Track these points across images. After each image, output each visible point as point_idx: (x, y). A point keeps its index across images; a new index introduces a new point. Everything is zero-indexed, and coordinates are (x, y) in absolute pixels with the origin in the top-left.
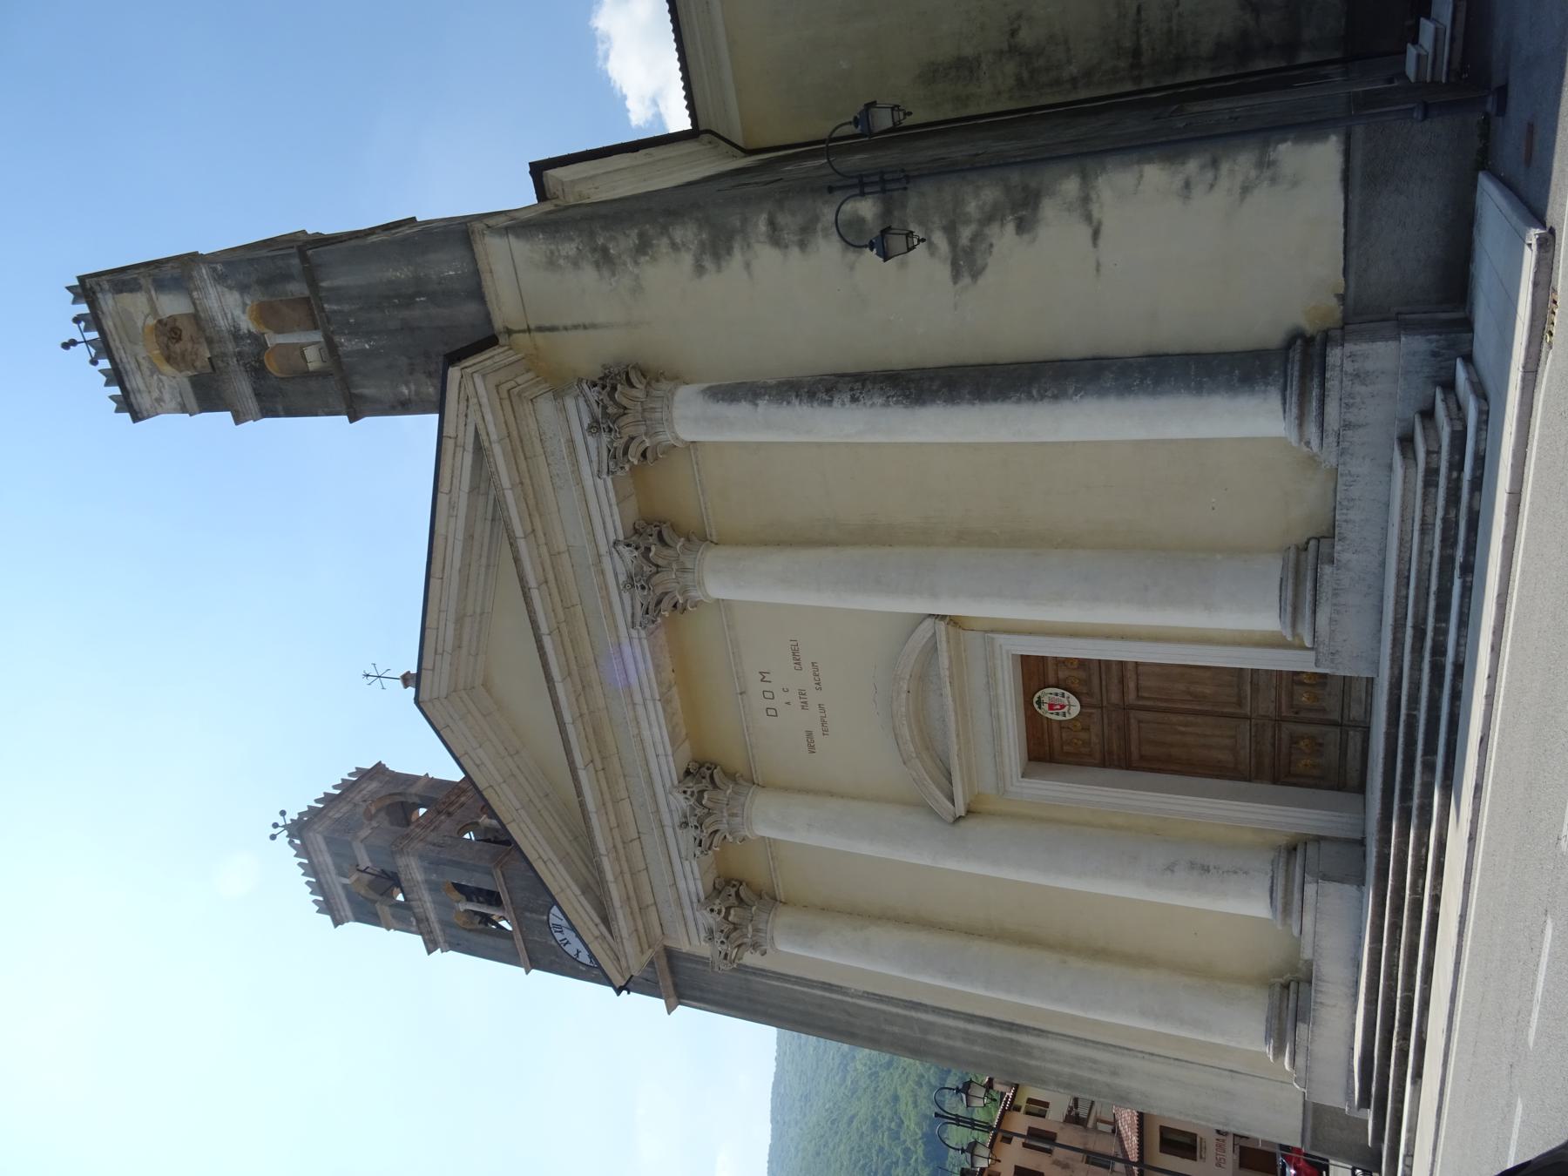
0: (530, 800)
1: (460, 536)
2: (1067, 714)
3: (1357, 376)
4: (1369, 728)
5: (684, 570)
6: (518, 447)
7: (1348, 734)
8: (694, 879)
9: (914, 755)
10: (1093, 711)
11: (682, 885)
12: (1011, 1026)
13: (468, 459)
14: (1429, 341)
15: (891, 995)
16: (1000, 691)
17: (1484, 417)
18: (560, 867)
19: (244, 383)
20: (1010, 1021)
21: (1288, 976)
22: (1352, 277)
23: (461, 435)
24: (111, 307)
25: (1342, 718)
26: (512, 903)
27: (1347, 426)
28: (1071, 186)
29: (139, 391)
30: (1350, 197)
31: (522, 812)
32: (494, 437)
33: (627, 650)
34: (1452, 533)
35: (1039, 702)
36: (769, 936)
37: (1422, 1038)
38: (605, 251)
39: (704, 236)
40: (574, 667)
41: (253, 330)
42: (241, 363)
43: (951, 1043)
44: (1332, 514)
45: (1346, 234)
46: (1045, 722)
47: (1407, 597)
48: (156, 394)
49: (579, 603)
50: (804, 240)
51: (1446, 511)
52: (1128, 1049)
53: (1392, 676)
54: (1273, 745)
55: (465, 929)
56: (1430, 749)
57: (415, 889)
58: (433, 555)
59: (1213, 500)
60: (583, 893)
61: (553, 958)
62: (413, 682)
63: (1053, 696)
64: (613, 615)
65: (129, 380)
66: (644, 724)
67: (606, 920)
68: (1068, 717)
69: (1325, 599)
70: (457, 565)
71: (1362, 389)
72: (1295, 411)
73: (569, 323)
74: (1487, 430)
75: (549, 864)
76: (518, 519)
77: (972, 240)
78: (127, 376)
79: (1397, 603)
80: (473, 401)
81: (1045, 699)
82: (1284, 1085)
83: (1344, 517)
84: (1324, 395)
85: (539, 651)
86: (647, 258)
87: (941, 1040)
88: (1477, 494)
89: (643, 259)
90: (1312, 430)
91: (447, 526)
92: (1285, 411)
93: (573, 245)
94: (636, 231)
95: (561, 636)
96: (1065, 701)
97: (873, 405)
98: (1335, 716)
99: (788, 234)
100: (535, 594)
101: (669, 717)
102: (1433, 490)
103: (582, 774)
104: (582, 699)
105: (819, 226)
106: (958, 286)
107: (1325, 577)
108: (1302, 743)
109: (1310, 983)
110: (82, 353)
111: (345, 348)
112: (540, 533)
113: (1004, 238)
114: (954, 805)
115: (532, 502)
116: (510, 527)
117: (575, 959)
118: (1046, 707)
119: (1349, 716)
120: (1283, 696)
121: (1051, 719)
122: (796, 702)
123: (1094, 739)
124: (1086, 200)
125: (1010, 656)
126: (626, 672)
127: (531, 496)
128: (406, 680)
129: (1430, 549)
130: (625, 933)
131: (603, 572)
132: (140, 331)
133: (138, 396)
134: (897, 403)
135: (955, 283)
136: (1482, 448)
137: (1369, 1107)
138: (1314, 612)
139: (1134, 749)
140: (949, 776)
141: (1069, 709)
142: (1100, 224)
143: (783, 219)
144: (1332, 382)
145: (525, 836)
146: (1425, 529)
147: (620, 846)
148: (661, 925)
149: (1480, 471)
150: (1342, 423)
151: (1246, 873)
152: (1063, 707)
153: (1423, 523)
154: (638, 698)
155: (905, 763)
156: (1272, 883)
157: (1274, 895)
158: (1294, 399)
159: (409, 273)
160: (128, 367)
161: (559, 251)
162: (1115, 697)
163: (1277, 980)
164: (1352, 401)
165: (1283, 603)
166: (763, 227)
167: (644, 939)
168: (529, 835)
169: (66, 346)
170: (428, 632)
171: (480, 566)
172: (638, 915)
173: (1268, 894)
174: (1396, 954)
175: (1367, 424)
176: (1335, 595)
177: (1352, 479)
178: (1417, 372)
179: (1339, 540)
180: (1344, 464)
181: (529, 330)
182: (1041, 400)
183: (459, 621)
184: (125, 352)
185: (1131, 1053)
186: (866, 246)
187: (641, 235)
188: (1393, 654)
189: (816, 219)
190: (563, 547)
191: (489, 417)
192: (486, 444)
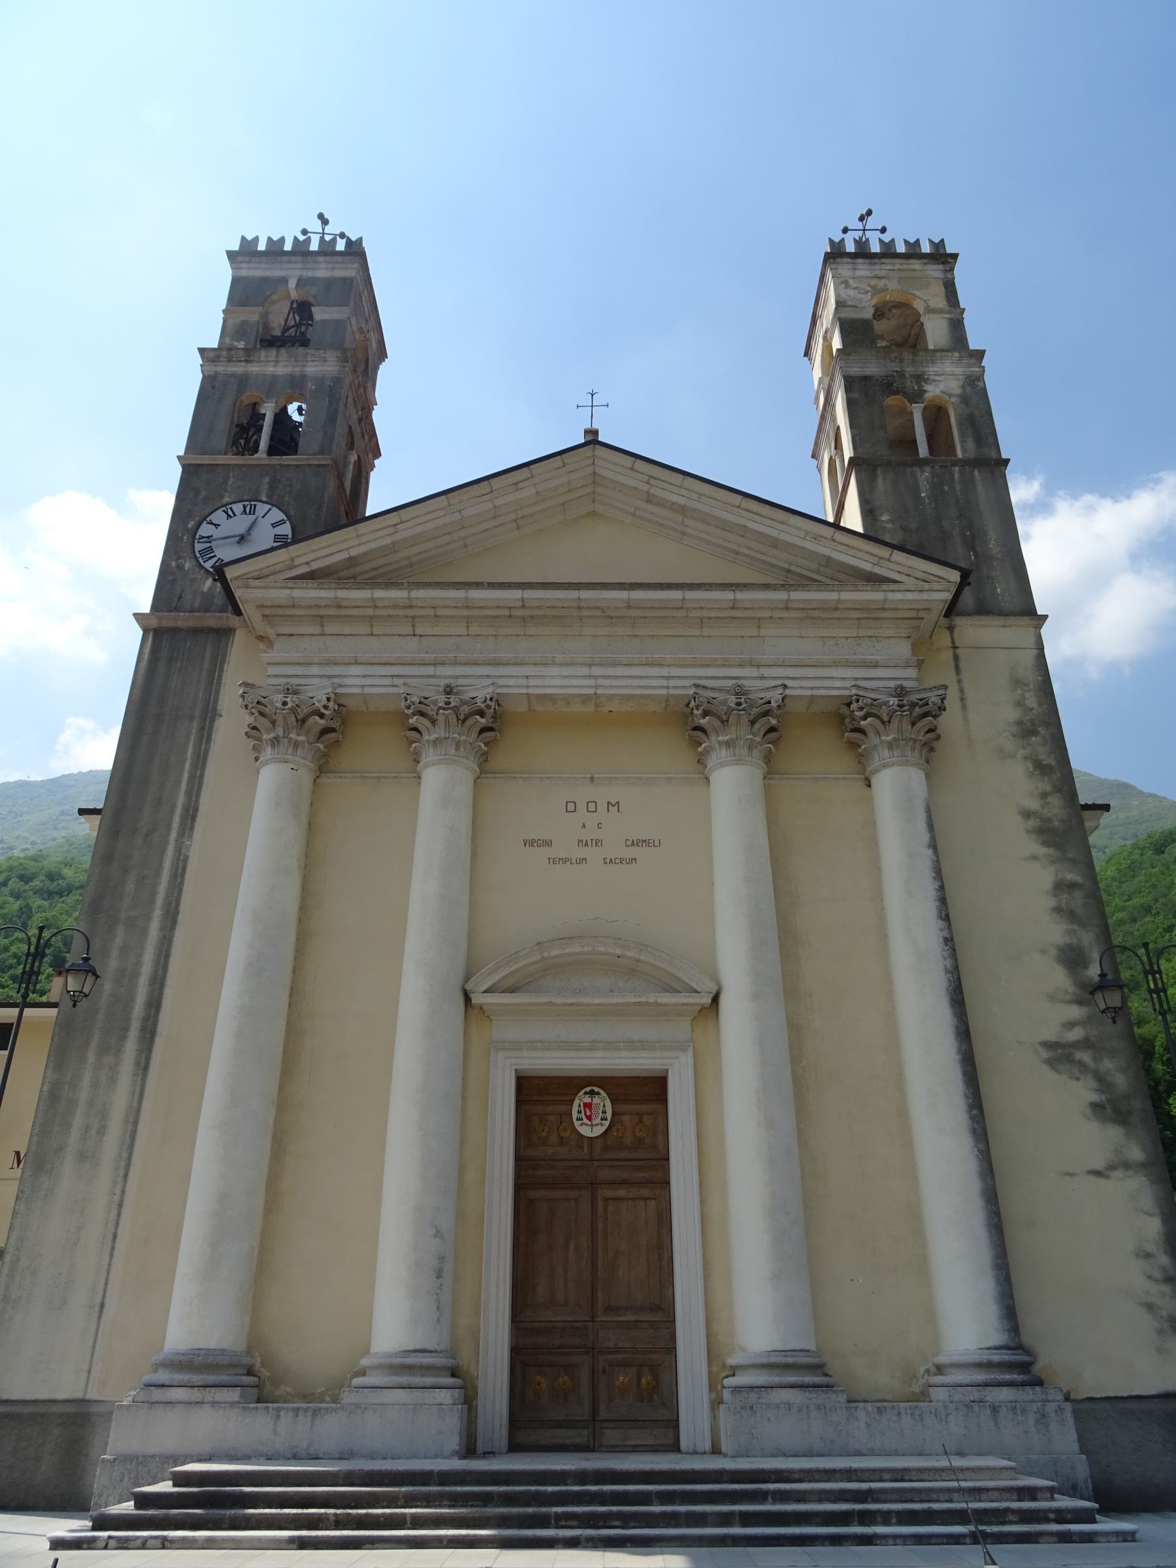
0: (463, 527)
1: (783, 536)
2: (580, 1122)
3: (1043, 1417)
4: (593, 1451)
5: (751, 747)
6: (870, 615)
7: (584, 1428)
8: (363, 686)
9: (545, 954)
10: (586, 1150)
11: (355, 670)
12: (149, 1032)
13: (867, 567)
14: (1086, 1480)
15: (185, 888)
16: (624, 1054)
17: (1130, 1538)
18: (388, 541)
19: (877, 370)
20: (159, 1030)
21: (265, 1373)
22: (1087, 1405)
23: (891, 565)
24: (931, 272)
25: (602, 1421)
26: (282, 466)
27: (995, 1409)
28: (1136, 1153)
29: (855, 269)
30: (1155, 1400)
31: (457, 516)
32: (890, 596)
33: (655, 671)
34: (993, 1519)
35: (592, 1093)
36: (289, 757)
37: (365, 1544)
38: (1032, 732)
39: (1056, 823)
40: (634, 613)
41: (927, 395)
42: (895, 373)
43: (115, 953)
44: (859, 1399)
45: (1122, 1398)
46: (568, 1098)
47: (881, 1480)
48: (851, 282)
49: (703, 634)
50: (1064, 912)
51: (1013, 1511)
52: (126, 1175)
53: (790, 1471)
54: (562, 1347)
55: (235, 402)
56: (747, 1519)
57: (293, 359)
58: (767, 506)
59: (861, 1280)
60: (350, 558)
61: (204, 493)
62: (590, 438)
64: (693, 666)
65: (864, 263)
66: (566, 671)
67: (311, 576)
68: (577, 1123)
69: (810, 1396)
71: (1031, 1422)
72: (996, 1358)
73: (965, 685)
74: (1117, 1542)
75: (392, 530)
77: (1080, 1063)
78: (869, 263)
79: (874, 1470)
80: (926, 586)
81: (596, 1100)
82: (85, 1375)
83: (903, 1411)
84: (1017, 1386)
85: (666, 583)
86: (1031, 769)
87: (118, 941)
88: (1055, 1539)
89: (1030, 765)
90: (981, 1376)
91: (798, 528)
92: (988, 1349)
93: (1034, 705)
94: (1053, 764)
95: (673, 608)
96: (597, 1121)
97: (945, 958)
98: (603, 1413)
99: (1066, 898)
100: (729, 595)
101: (567, 699)
102: (1015, 1497)
103: (517, 594)
104: (598, 613)
105: (1076, 927)
106: (1038, 1047)
107: (834, 1396)
108: (566, 1378)
109: (258, 1401)
111: (919, 474)
112: (784, 614)
113: (1085, 1092)
114: (485, 992)
115: (816, 614)
116: (801, 588)
117: (205, 519)
118: (587, 1100)
119: (607, 1428)
120: (622, 1356)
121: (572, 1104)
122: (586, 835)
123: (550, 1151)
124: (1126, 1165)
125: (666, 1067)
126: (628, 665)
127: (822, 615)
128: (592, 434)
129: (955, 1499)
130: (297, 593)
131: (741, 666)
132: (911, 291)
133: (850, 266)
134: (950, 981)
135: (1041, 1044)
136: (1100, 1539)
137: (175, 1485)
138: (792, 1386)
139: (541, 1193)
140: (512, 990)
141: (587, 1125)
142: (1108, 1177)
144: (1031, 1393)
145: (428, 513)
146: (976, 1493)
147: (411, 612)
148: (292, 635)
149: (1078, 1540)
150: (997, 1404)
151: (438, 1321)
152: (589, 1118)
153: (980, 1490)
154: (597, 671)
155: (538, 943)
156: (431, 1352)
157: (419, 1354)
158: (1006, 1358)
159: (994, 552)
160: (877, 267)
161: (1028, 691)
162: (605, 1174)
163: (259, 1360)
164: (1019, 1412)
165: (790, 1353)
166: (1070, 877)
167: (280, 612)
169: (869, 213)
170: (681, 477)
171: (740, 546)
172: (314, 612)
173: (418, 1347)
174: (445, 1503)
175: (999, 1428)
176: (819, 1408)
177: (943, 1417)
178: (1056, 1472)
179: (878, 1408)
180: (957, 1409)
181: (955, 648)
182: (970, 1118)
183: (683, 510)
184: (890, 270)
185: (120, 1178)
186: (1102, 970)
187: (1050, 767)
188: (818, 1471)
189: (1083, 925)
190: (763, 632)
191: (909, 596)
192: (884, 587)
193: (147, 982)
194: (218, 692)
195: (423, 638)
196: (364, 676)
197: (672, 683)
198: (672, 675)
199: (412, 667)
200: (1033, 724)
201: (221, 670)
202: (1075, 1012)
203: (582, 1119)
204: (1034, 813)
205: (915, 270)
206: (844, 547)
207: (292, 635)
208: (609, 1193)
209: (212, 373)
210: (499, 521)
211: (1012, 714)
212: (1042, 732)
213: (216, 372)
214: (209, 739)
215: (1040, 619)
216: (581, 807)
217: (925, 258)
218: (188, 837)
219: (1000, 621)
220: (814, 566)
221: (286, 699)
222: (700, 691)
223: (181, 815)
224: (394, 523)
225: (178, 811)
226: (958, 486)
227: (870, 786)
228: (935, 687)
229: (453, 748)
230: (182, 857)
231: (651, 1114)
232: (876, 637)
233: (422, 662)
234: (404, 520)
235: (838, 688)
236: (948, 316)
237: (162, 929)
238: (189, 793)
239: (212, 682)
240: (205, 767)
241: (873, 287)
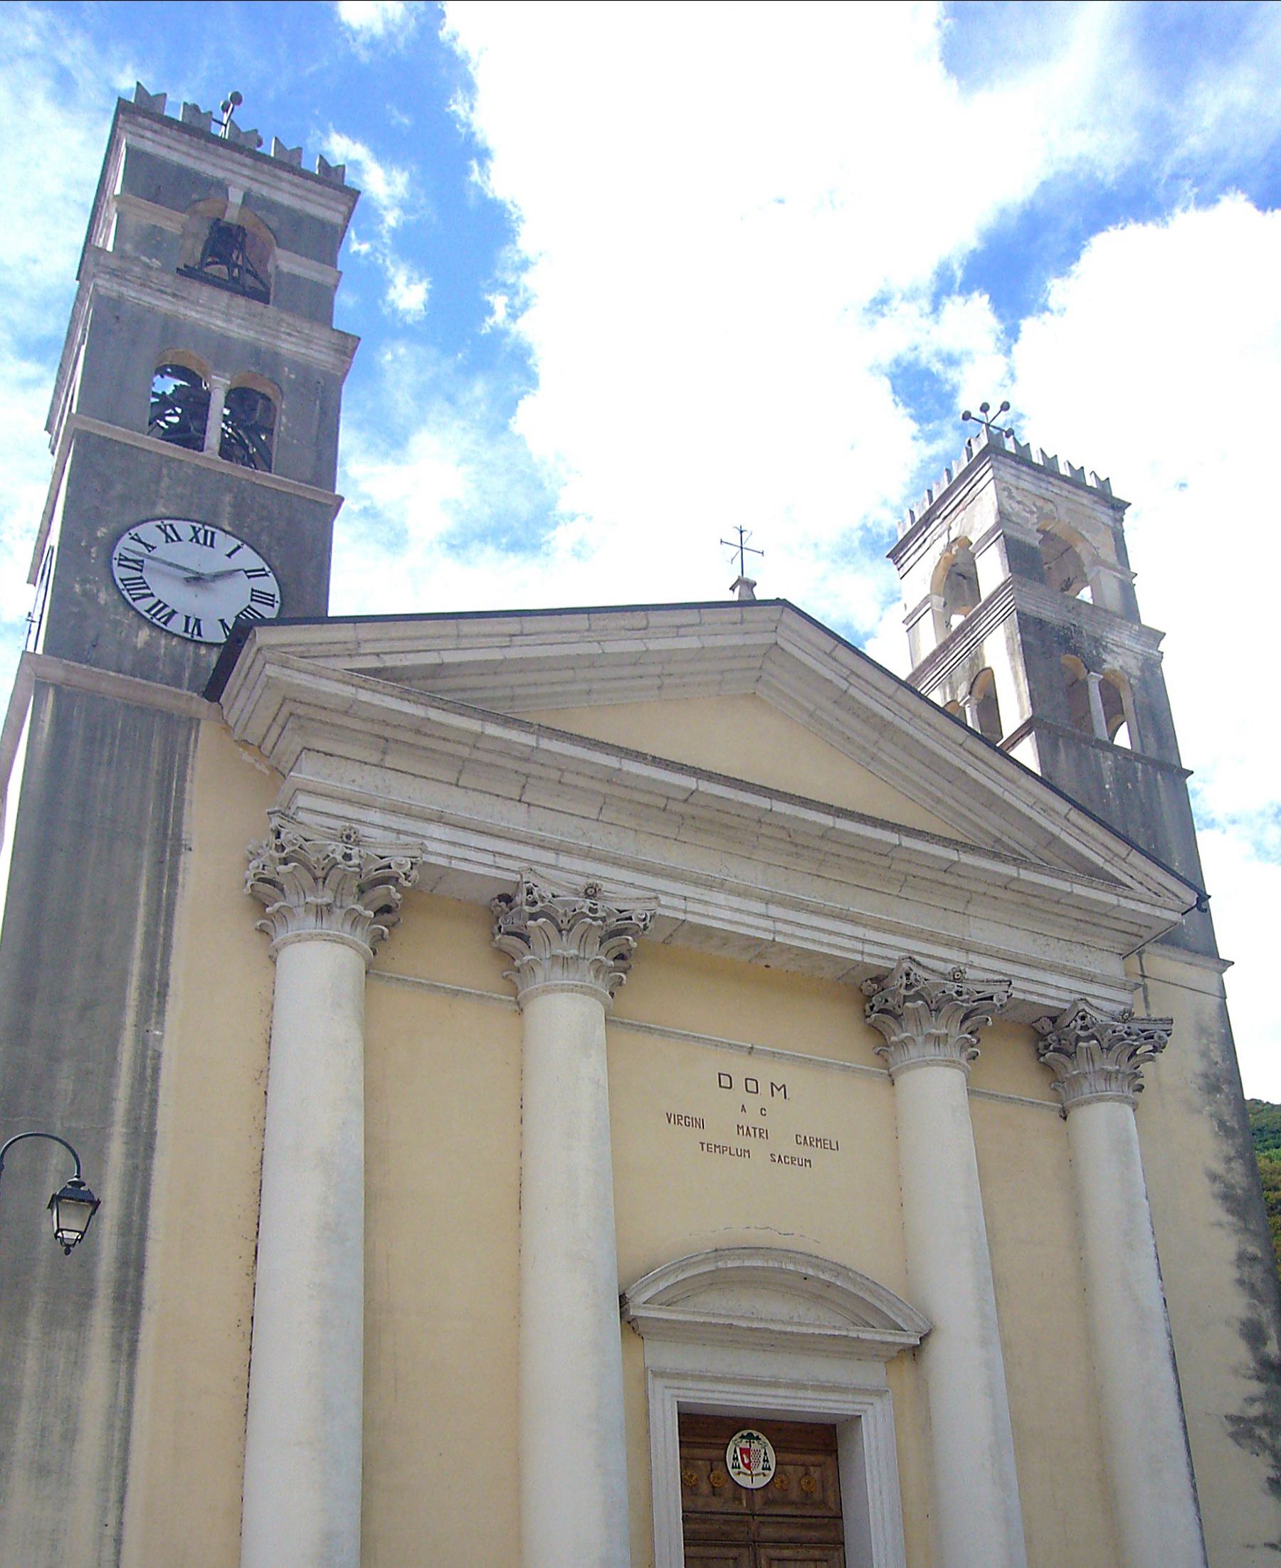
33: (847, 929)
35: (750, 1436)
40: (827, 846)
42: (1072, 627)
49: (900, 895)
61: (119, 488)
63: (763, 1455)
65: (1029, 474)
66: (735, 902)
70: (970, 770)
76: (1035, 880)
81: (755, 1446)
86: (1217, 1129)
89: (1215, 1123)
94: (1237, 1127)
110: (211, 103)
112: (999, 893)
141: (745, 1474)
143: (1258, 1268)
147: (525, 768)
152: (748, 1466)
154: (775, 911)
162: (768, 1532)
167: (323, 715)
168: (559, 638)
169: (237, 99)
172: (378, 729)
184: (1056, 494)
189: (1262, 1302)
190: (971, 909)
192: (1119, 891)
193: (115, 1230)
194: (179, 809)
195: (532, 808)
196: (454, 844)
197: (868, 948)
198: (867, 938)
199: (521, 847)
200: (1218, 1080)
201: (182, 778)
202: (1256, 1388)
203: (739, 1467)
204: (1220, 1177)
205: (1083, 505)
206: (1077, 831)
207: (331, 755)
208: (774, 1553)
209: (114, 294)
210: (639, 671)
211: (1198, 1065)
212: (1226, 1090)
213: (121, 296)
214: (173, 881)
215: (1224, 965)
216: (739, 1083)
217: (1096, 495)
218: (157, 1023)
219: (1188, 957)
220: (1031, 843)
221: (348, 851)
222: (915, 969)
223: (140, 988)
224: (512, 633)
225: (134, 983)
226: (1141, 787)
227: (1065, 1118)
228: (1161, 1020)
229: (592, 973)
230: (150, 1053)
231: (819, 1465)
232: (1088, 946)
233: (541, 844)
234: (526, 632)
235: (1052, 998)
236: (1119, 575)
237: (130, 1155)
238: (149, 956)
239: (169, 792)
240: (172, 922)
241: (1040, 509)
